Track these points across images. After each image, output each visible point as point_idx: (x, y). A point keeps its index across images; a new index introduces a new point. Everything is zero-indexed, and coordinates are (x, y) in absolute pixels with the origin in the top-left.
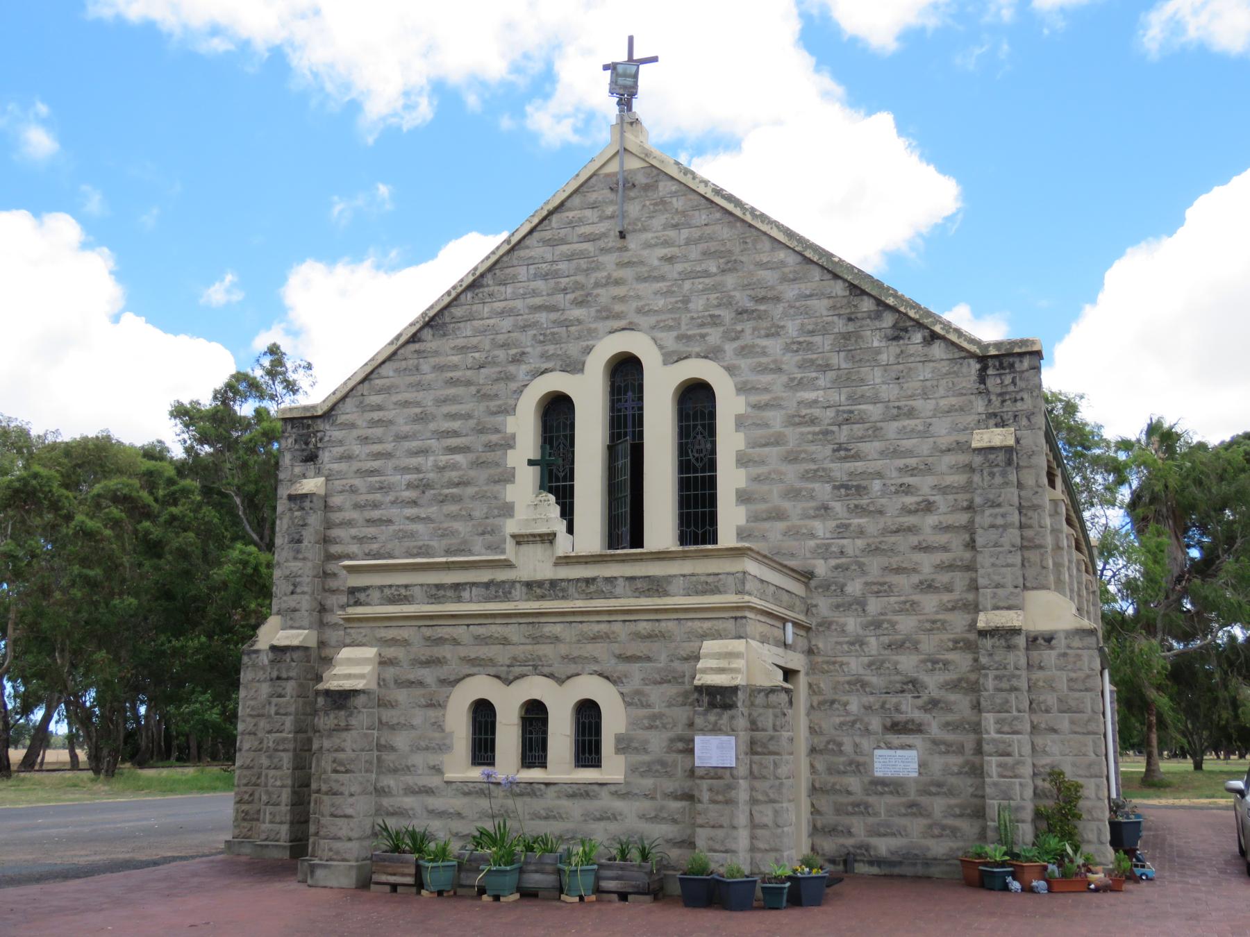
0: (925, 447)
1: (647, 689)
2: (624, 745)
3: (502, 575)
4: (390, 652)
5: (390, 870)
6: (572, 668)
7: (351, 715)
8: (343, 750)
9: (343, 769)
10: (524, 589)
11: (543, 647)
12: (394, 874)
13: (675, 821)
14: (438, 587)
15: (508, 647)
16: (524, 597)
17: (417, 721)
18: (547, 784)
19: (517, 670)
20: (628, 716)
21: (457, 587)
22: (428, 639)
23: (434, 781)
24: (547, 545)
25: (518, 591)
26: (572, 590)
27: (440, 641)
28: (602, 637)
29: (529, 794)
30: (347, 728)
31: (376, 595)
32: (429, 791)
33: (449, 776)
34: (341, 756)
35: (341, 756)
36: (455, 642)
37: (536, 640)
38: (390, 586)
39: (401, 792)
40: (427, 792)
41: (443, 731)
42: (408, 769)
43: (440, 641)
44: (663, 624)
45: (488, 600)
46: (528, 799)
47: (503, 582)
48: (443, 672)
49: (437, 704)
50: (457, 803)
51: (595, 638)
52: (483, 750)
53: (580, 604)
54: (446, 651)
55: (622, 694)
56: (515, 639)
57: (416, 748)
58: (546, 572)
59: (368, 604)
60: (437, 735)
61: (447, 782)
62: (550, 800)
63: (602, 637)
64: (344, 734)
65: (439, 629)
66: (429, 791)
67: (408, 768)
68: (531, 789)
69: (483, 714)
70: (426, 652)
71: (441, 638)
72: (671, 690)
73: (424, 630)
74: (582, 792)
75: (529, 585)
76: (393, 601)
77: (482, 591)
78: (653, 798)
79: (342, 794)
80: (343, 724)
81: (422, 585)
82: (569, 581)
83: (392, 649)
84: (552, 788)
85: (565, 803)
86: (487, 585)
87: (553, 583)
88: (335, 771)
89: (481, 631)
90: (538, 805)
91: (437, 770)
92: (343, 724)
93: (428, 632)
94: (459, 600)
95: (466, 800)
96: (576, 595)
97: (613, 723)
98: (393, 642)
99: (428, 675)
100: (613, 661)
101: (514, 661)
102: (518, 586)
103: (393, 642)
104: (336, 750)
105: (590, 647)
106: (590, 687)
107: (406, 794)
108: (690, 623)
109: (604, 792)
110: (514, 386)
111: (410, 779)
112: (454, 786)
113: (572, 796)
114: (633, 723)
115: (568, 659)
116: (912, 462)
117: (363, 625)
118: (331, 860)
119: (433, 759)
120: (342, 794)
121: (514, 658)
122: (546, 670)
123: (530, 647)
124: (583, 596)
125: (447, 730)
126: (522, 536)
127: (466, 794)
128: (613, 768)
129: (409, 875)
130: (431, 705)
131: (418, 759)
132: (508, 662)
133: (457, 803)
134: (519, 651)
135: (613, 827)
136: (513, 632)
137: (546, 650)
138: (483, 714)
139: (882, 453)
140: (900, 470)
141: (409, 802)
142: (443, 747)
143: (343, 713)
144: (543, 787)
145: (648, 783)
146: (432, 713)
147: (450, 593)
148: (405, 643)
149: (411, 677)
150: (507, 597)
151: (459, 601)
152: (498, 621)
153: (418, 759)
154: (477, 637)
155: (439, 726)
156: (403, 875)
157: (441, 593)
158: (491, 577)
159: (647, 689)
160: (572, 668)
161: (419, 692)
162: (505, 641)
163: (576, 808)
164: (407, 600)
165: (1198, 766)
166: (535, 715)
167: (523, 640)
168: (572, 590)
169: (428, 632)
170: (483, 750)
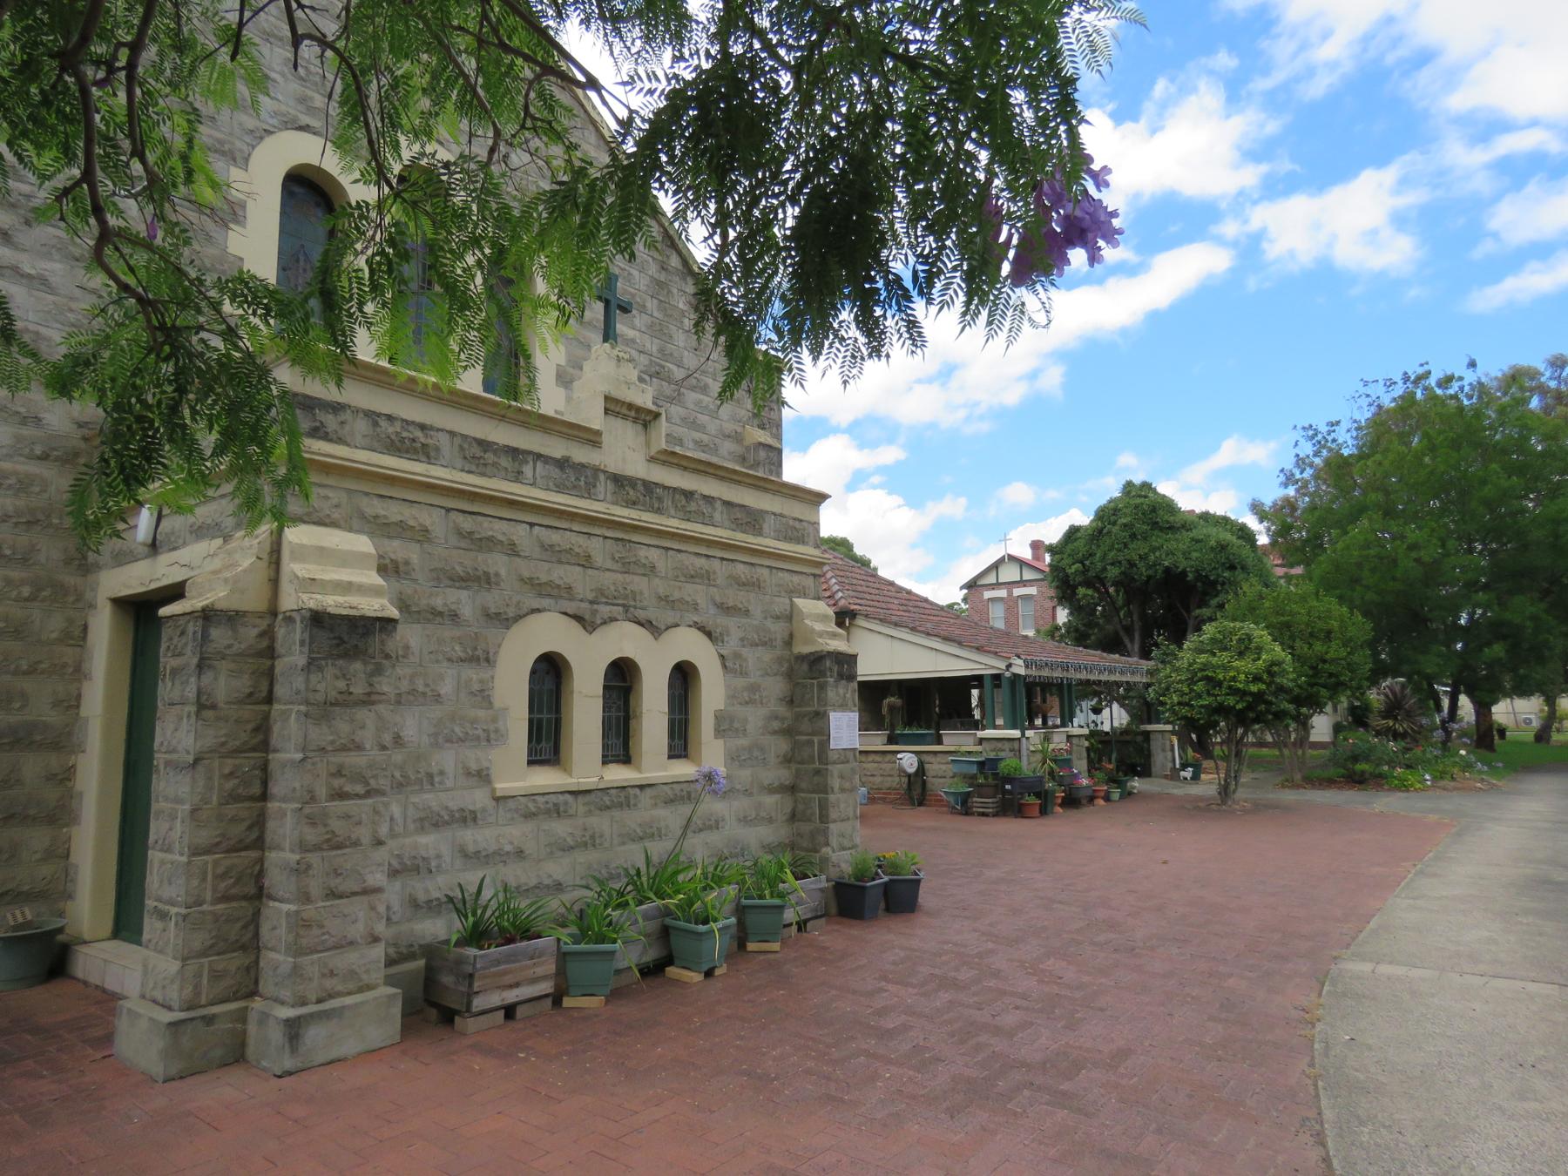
0: (712, 427)
1: (745, 652)
2: (725, 725)
3: (580, 454)
4: (397, 549)
5: (508, 979)
6: (670, 617)
7: (378, 670)
8: (359, 747)
9: (360, 789)
10: (610, 486)
11: (637, 579)
12: (517, 985)
13: (770, 820)
14: (484, 445)
15: (590, 572)
16: (609, 496)
17: (446, 688)
18: (641, 787)
19: (605, 610)
20: (727, 687)
21: (514, 452)
22: (461, 534)
23: (478, 798)
24: (640, 427)
25: (603, 487)
26: (667, 503)
27: (487, 544)
28: (702, 577)
29: (620, 805)
30: (368, 700)
31: (361, 426)
32: (468, 818)
33: (503, 786)
34: (353, 760)
35: (353, 760)
36: (512, 550)
37: (627, 567)
38: (390, 418)
39: (412, 827)
40: (464, 820)
41: (490, 705)
42: (431, 780)
43: (487, 544)
44: (759, 570)
45: (560, 488)
46: (616, 813)
47: (583, 465)
48: (493, 600)
49: (484, 658)
50: (515, 833)
51: (692, 577)
52: (547, 742)
53: (673, 524)
54: (497, 563)
55: (722, 657)
56: (598, 559)
57: (443, 738)
58: (637, 467)
59: (340, 441)
60: (481, 713)
61: (497, 799)
62: (645, 812)
63: (702, 577)
64: (362, 714)
65: (486, 522)
66: (468, 818)
67: (430, 776)
68: (623, 797)
69: (551, 672)
70: (463, 561)
71: (490, 539)
72: (767, 656)
73: (460, 518)
74: (680, 794)
75: (619, 480)
76: (396, 447)
77: (555, 472)
78: (751, 794)
79: (356, 843)
80: (358, 689)
81: (452, 434)
82: (665, 488)
83: (396, 543)
84: (648, 791)
85: (661, 812)
86: (563, 463)
87: (649, 487)
88: (341, 795)
89: (555, 538)
90: (633, 819)
91: (483, 777)
92: (358, 689)
93: (467, 523)
94: (518, 477)
95: (529, 827)
96: (672, 512)
97: (712, 694)
98: (399, 530)
99: (465, 602)
100: (713, 610)
101: (600, 597)
102: (602, 477)
103: (399, 530)
104: (344, 749)
105: (689, 588)
106: (688, 645)
107: (422, 830)
108: (780, 574)
109: (645, 798)
110: (250, 122)
111: (431, 800)
112: (511, 804)
113: (669, 802)
114: (732, 697)
115: (666, 601)
116: (705, 438)
117: (330, 481)
118: (332, 996)
119: (473, 757)
120: (356, 843)
121: (601, 592)
122: (641, 614)
123: (620, 576)
124: (680, 514)
125: (497, 704)
126: (617, 401)
127: (529, 816)
128: (712, 753)
129: (544, 978)
130: (473, 660)
131: (447, 760)
132: (590, 596)
133: (515, 833)
134: (609, 580)
135: (715, 838)
136: (597, 548)
137: (639, 583)
138: (551, 672)
139: (684, 419)
140: (696, 442)
141: (429, 842)
142: (491, 737)
143: (357, 666)
144: (637, 791)
145: (745, 774)
146: (472, 673)
147: (505, 462)
148: (422, 535)
149: (438, 602)
150: (588, 492)
151: (517, 480)
152: (576, 527)
153: (447, 760)
154: (547, 548)
155: (483, 696)
156: (535, 980)
157: (490, 457)
158: (566, 453)
159: (745, 652)
160: (670, 617)
161: (448, 632)
162: (586, 562)
163: (672, 818)
164: (426, 453)
165: (1023, 734)
166: (622, 676)
167: (609, 564)
168: (667, 503)
169: (467, 523)
170: (547, 742)
